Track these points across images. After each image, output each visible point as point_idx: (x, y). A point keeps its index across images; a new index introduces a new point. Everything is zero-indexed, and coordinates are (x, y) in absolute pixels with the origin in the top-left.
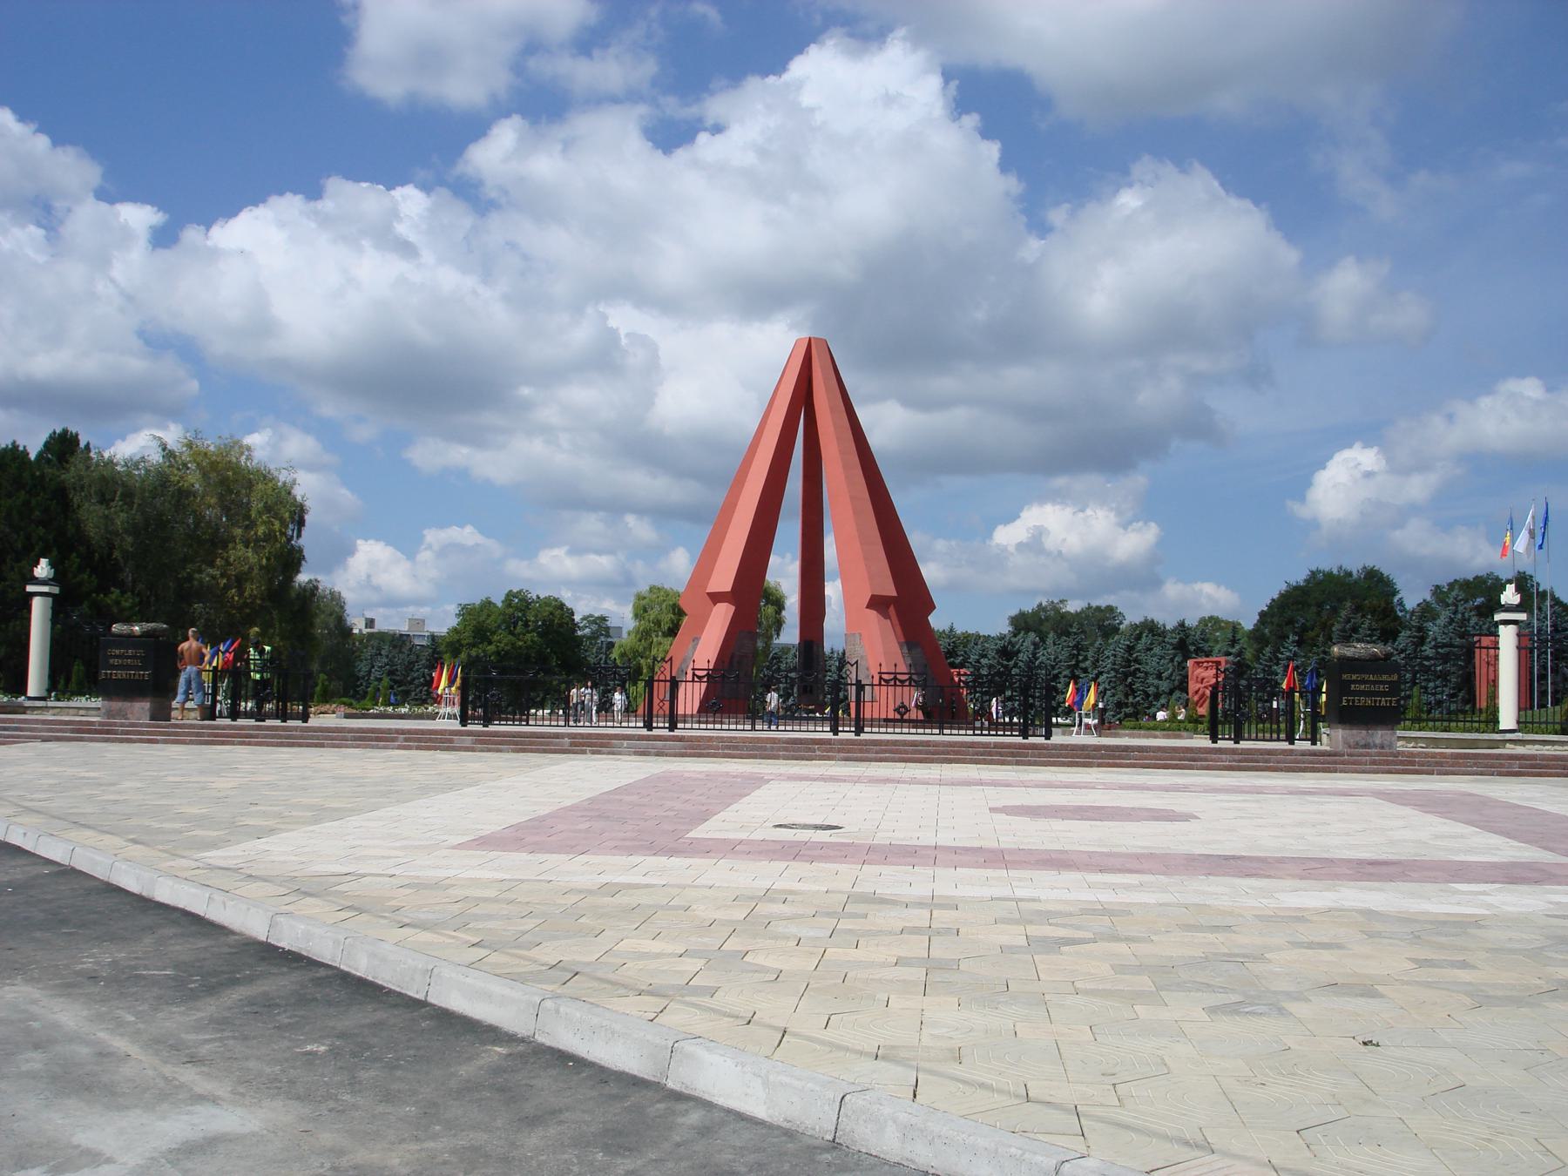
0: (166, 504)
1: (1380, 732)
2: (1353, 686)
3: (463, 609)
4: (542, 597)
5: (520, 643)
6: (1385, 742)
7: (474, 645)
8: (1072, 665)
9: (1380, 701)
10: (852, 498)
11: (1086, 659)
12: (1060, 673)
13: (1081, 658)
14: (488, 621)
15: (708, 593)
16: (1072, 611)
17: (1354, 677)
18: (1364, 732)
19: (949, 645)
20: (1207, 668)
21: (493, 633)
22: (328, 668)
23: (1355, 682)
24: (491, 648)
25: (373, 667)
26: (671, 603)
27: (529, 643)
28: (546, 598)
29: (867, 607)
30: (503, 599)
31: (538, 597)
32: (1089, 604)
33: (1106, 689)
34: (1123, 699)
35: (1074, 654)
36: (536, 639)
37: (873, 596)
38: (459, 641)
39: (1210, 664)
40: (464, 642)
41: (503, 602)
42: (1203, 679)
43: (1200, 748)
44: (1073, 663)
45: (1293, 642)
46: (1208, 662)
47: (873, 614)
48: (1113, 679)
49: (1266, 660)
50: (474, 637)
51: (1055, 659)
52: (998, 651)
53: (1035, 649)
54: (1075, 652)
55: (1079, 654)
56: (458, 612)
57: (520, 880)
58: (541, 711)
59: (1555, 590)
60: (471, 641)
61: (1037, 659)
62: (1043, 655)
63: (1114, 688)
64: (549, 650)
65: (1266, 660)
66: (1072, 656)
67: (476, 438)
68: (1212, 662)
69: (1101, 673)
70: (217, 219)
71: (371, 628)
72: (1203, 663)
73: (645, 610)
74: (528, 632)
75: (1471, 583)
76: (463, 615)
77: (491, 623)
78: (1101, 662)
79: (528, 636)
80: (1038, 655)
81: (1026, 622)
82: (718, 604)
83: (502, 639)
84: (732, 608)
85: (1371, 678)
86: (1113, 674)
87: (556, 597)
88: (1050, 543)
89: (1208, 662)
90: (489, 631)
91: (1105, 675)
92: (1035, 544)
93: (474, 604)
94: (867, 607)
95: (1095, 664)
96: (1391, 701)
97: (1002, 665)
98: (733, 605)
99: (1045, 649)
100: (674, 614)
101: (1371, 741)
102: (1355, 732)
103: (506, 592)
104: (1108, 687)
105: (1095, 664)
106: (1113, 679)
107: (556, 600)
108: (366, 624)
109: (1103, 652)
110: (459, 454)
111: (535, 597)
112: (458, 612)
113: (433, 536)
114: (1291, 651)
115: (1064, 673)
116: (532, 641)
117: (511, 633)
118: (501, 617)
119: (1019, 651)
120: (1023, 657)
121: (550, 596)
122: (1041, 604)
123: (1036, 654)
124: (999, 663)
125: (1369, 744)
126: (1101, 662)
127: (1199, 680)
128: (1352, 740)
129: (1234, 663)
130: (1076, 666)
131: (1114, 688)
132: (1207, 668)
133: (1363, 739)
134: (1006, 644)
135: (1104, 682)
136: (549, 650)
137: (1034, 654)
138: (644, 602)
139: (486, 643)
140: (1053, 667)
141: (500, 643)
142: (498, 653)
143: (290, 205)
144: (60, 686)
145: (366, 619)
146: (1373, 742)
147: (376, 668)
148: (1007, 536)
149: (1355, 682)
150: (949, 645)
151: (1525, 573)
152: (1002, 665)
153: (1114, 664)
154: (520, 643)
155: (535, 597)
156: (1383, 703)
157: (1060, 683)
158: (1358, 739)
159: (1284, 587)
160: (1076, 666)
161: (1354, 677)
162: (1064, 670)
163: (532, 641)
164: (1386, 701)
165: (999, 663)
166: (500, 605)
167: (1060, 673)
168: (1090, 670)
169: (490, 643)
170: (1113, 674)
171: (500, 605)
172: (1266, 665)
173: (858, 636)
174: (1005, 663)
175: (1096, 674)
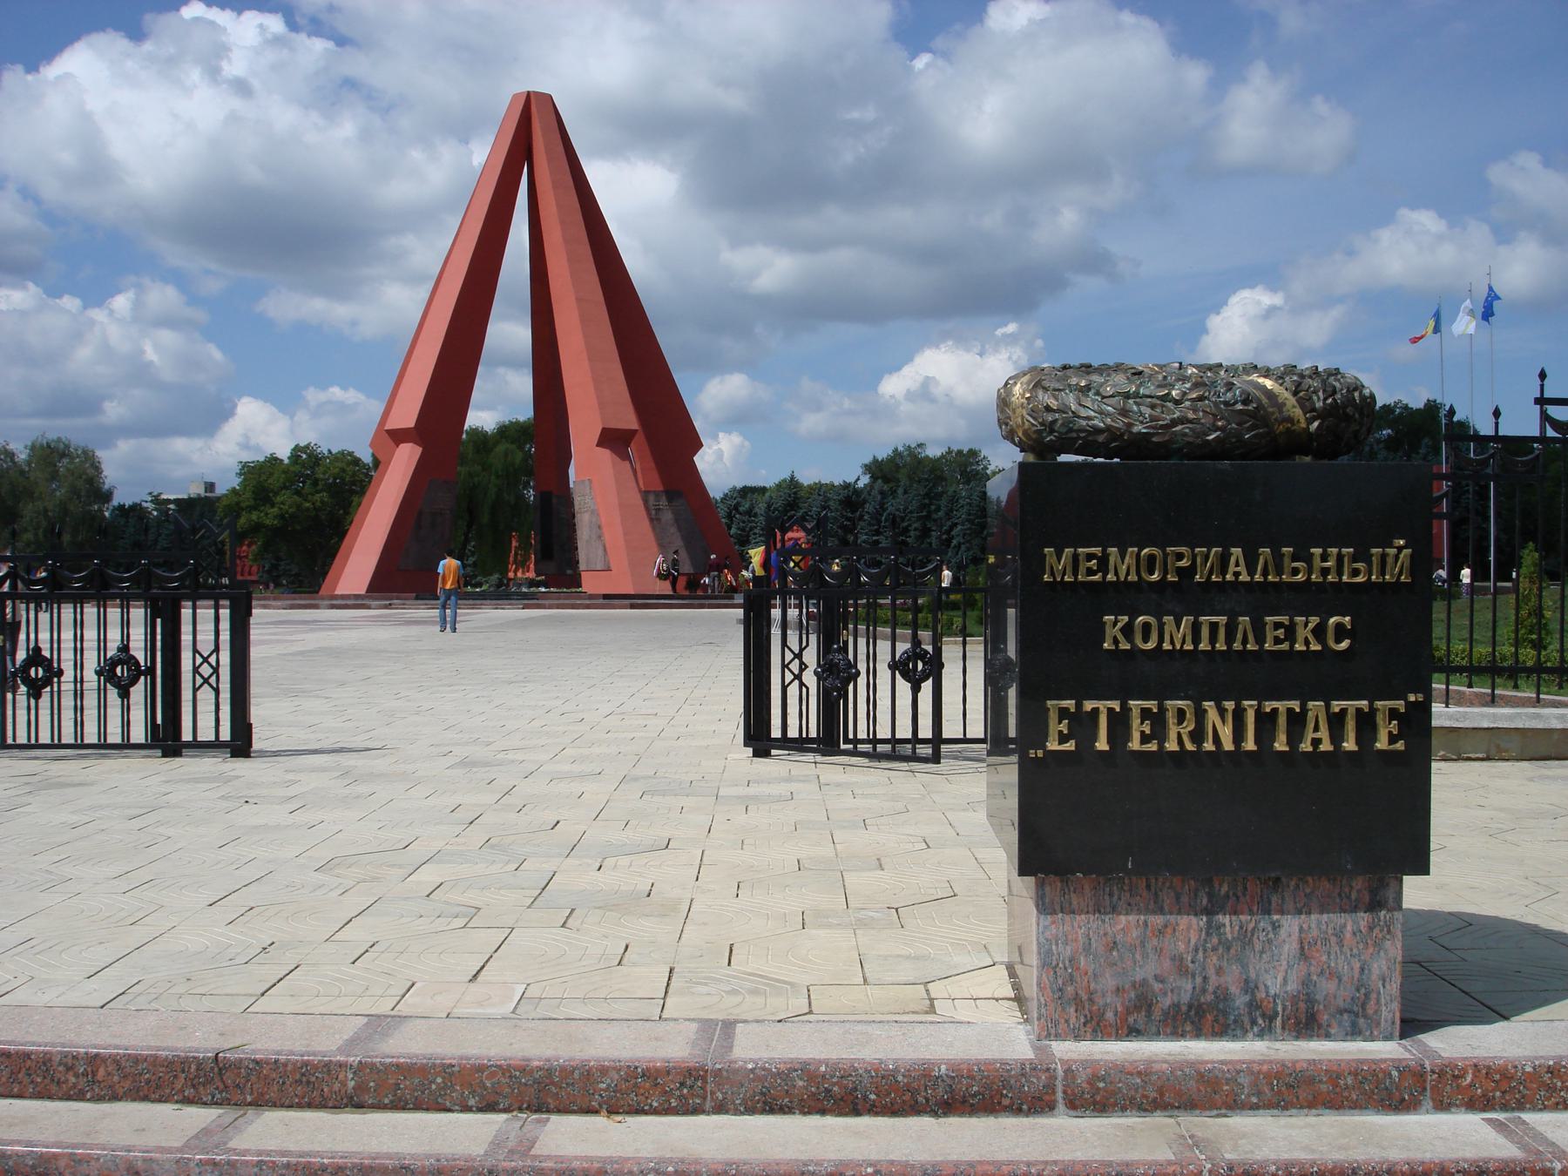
1: (1290, 925)
2: (1113, 624)
3: (243, 467)
4: (334, 452)
5: (308, 505)
6: (1326, 987)
7: (255, 508)
8: (922, 517)
9: (1119, 723)
10: (578, 300)
11: (938, 509)
12: (910, 525)
13: (933, 507)
14: (270, 481)
15: (388, 431)
16: (931, 456)
17: (1123, 565)
18: (1190, 926)
19: (790, 496)
21: (276, 494)
22: (80, 538)
23: (1127, 597)
24: (275, 510)
25: (160, 535)
27: (318, 504)
29: (597, 446)
30: (289, 454)
31: (330, 451)
32: (949, 448)
33: (960, 544)
34: (979, 553)
35: (926, 504)
36: (326, 499)
37: (604, 429)
38: (238, 504)
40: (243, 505)
41: (289, 458)
43: (94, 1060)
44: (924, 513)
47: (605, 454)
48: (968, 532)
50: (255, 499)
51: (904, 510)
52: (841, 502)
53: (883, 498)
54: (927, 501)
55: (931, 504)
56: (238, 472)
57: (292, 780)
60: (252, 502)
61: (884, 510)
62: (892, 505)
63: (968, 541)
64: (341, 512)
66: (923, 507)
67: (339, 291)
69: (956, 525)
70: (883, 377)
71: (211, 492)
74: (318, 492)
76: (244, 474)
77: (274, 482)
78: (955, 512)
79: (317, 497)
80: (886, 506)
81: (881, 470)
82: (402, 445)
83: (286, 500)
84: (418, 450)
85: (1237, 568)
86: (968, 525)
88: (937, 391)
90: (272, 491)
91: (959, 527)
92: (924, 392)
94: (597, 446)
95: (948, 514)
96: (1366, 723)
97: (848, 519)
98: (420, 446)
99: (894, 498)
101: (1232, 980)
102: (1126, 924)
104: (962, 541)
105: (948, 514)
106: (968, 532)
108: (206, 488)
109: (957, 501)
110: (317, 307)
111: (326, 453)
112: (238, 472)
113: (313, 396)
115: (915, 525)
116: (322, 502)
117: (298, 493)
119: (865, 502)
120: (869, 507)
121: (343, 451)
122: (896, 449)
123: (884, 504)
124: (843, 516)
125: (1223, 996)
126: (955, 512)
128: (1109, 981)
130: (928, 517)
131: (968, 541)
133: (1182, 969)
134: (850, 493)
135: (958, 535)
136: (341, 512)
137: (882, 505)
139: (268, 505)
140: (903, 519)
141: (284, 504)
142: (282, 517)
143: (112, 43)
145: (206, 483)
146: (1249, 987)
147: (163, 536)
148: (894, 386)
149: (1127, 597)
150: (790, 496)
151: (1435, 401)
152: (848, 519)
153: (970, 514)
154: (308, 505)
155: (326, 453)
156: (1317, 737)
157: (910, 537)
158: (1146, 970)
160: (928, 517)
161: (1123, 565)
162: (914, 523)
163: (322, 502)
164: (1336, 722)
165: (843, 516)
166: (286, 461)
167: (910, 525)
169: (273, 505)
170: (968, 525)
171: (286, 461)
173: (587, 483)
174: (850, 515)
175: (950, 526)
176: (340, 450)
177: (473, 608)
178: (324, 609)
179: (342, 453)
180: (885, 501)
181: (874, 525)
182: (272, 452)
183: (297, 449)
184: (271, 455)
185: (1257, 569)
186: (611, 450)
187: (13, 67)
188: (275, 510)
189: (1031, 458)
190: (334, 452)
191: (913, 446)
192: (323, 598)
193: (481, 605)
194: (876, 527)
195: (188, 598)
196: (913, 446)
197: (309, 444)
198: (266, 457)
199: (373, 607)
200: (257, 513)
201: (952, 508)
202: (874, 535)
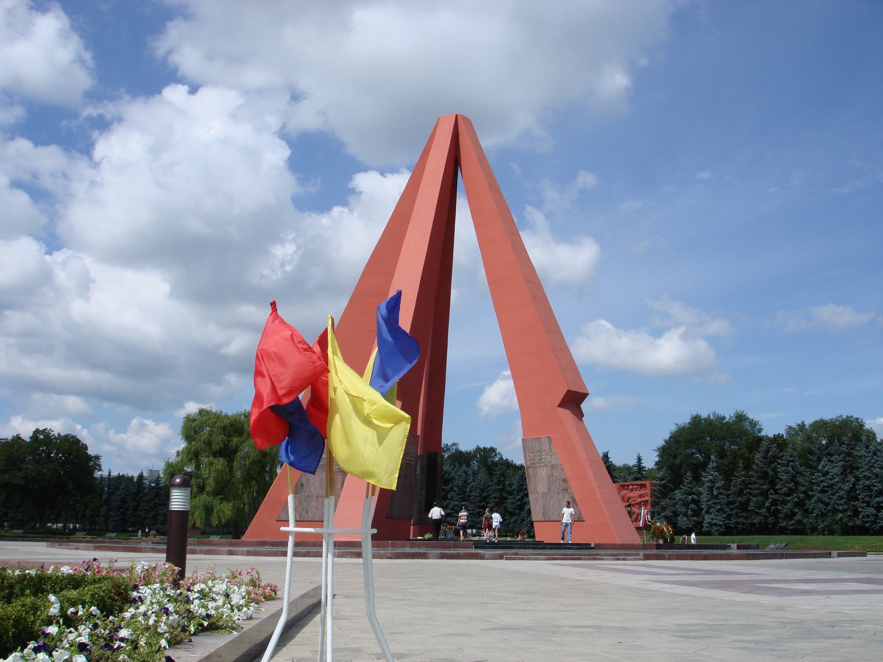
0: (43, 609)
20: (632, 490)
24: (21, 474)
26: (222, 425)
28: (65, 436)
29: (561, 405)
37: (568, 390)
39: (635, 486)
42: (629, 499)
45: (713, 468)
46: (633, 485)
49: (688, 483)
51: (484, 484)
58: (56, 525)
59: (609, 452)
65: (688, 483)
68: (637, 485)
72: (628, 486)
73: (196, 432)
75: (828, 423)
87: (73, 435)
89: (633, 485)
93: (7, 439)
100: (225, 435)
103: (34, 430)
107: (73, 437)
111: (56, 435)
114: (712, 475)
115: (494, 495)
118: (30, 449)
119: (453, 479)
127: (626, 499)
129: (660, 485)
130: (503, 489)
132: (632, 490)
138: (194, 424)
144: (453, 520)
155: (56, 435)
159: (674, 428)
168: (515, 493)
169: (20, 470)
172: (689, 487)
176: (66, 434)
177: (594, 559)
178: (434, 558)
179: (67, 436)
180: (467, 478)
181: (461, 495)
182: (17, 433)
183: (37, 431)
184: (17, 435)
185: (460, 535)
186: (571, 411)
187: (175, 85)
188: (21, 474)
189: (135, 480)
190: (62, 435)
191: (449, 445)
192: (246, 544)
193: (597, 555)
194: (462, 496)
195: (169, 540)
196: (449, 445)
197: (46, 429)
198: (14, 436)
199: (486, 556)
200: (8, 475)
201: (522, 484)
202: (461, 502)
